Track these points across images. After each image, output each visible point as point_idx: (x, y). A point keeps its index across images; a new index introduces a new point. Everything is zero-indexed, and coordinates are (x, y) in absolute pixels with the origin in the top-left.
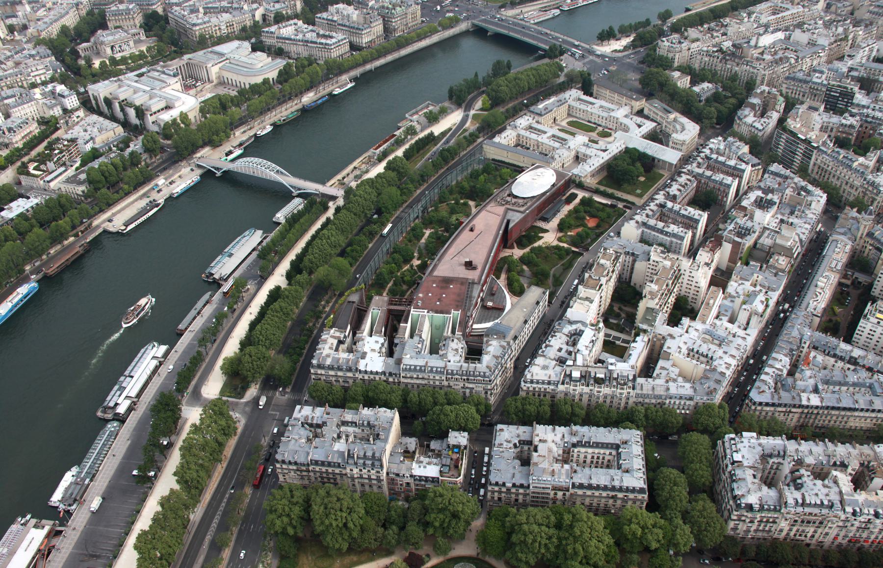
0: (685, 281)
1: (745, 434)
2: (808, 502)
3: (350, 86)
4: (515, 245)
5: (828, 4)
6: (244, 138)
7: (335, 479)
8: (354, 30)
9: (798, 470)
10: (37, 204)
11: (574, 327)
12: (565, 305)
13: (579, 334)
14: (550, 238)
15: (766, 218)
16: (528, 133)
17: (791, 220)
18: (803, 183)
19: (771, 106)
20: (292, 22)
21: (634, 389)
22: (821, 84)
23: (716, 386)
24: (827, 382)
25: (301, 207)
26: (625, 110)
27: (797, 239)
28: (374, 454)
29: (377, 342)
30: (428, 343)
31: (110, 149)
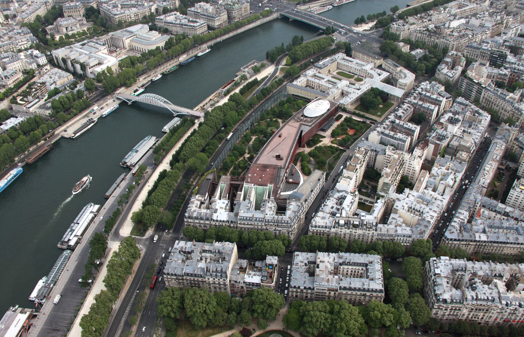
0: (407, 167)
1: (442, 257)
2: (479, 298)
3: (208, 51)
4: (306, 145)
5: (491, 2)
6: (145, 82)
7: (199, 284)
8: (210, 18)
9: (473, 279)
10: (22, 121)
11: (341, 194)
12: (335, 181)
13: (343, 198)
14: (326, 141)
15: (455, 130)
16: (313, 79)
17: (469, 131)
18: (477, 109)
19: (457, 63)
20: (173, 13)
21: (376, 231)
22: (487, 50)
23: (425, 229)
24: (491, 227)
25: (178, 123)
26: (371, 66)
27: (473, 142)
28: (222, 269)
29: (224, 203)
30: (254, 203)
31: (66, 89)
